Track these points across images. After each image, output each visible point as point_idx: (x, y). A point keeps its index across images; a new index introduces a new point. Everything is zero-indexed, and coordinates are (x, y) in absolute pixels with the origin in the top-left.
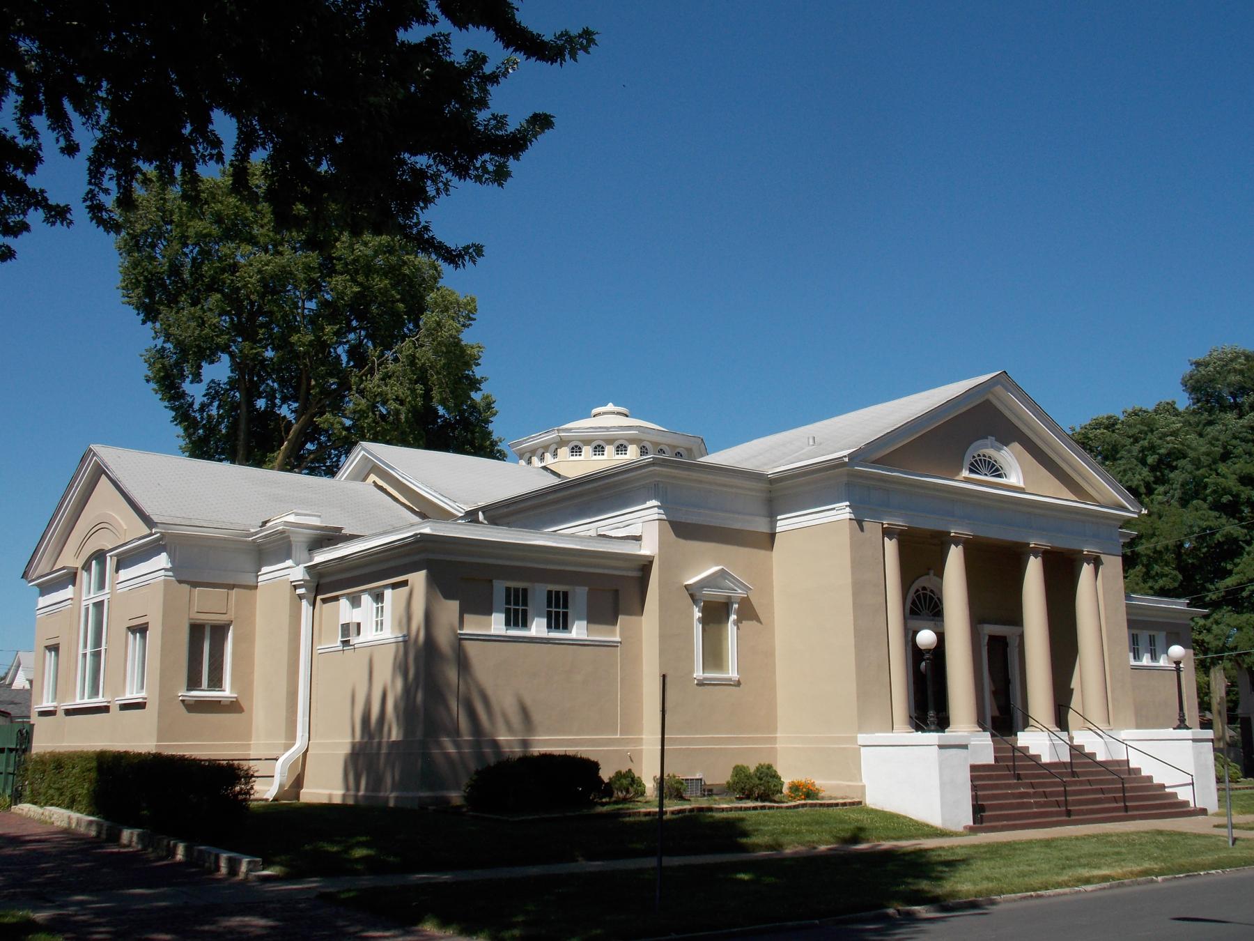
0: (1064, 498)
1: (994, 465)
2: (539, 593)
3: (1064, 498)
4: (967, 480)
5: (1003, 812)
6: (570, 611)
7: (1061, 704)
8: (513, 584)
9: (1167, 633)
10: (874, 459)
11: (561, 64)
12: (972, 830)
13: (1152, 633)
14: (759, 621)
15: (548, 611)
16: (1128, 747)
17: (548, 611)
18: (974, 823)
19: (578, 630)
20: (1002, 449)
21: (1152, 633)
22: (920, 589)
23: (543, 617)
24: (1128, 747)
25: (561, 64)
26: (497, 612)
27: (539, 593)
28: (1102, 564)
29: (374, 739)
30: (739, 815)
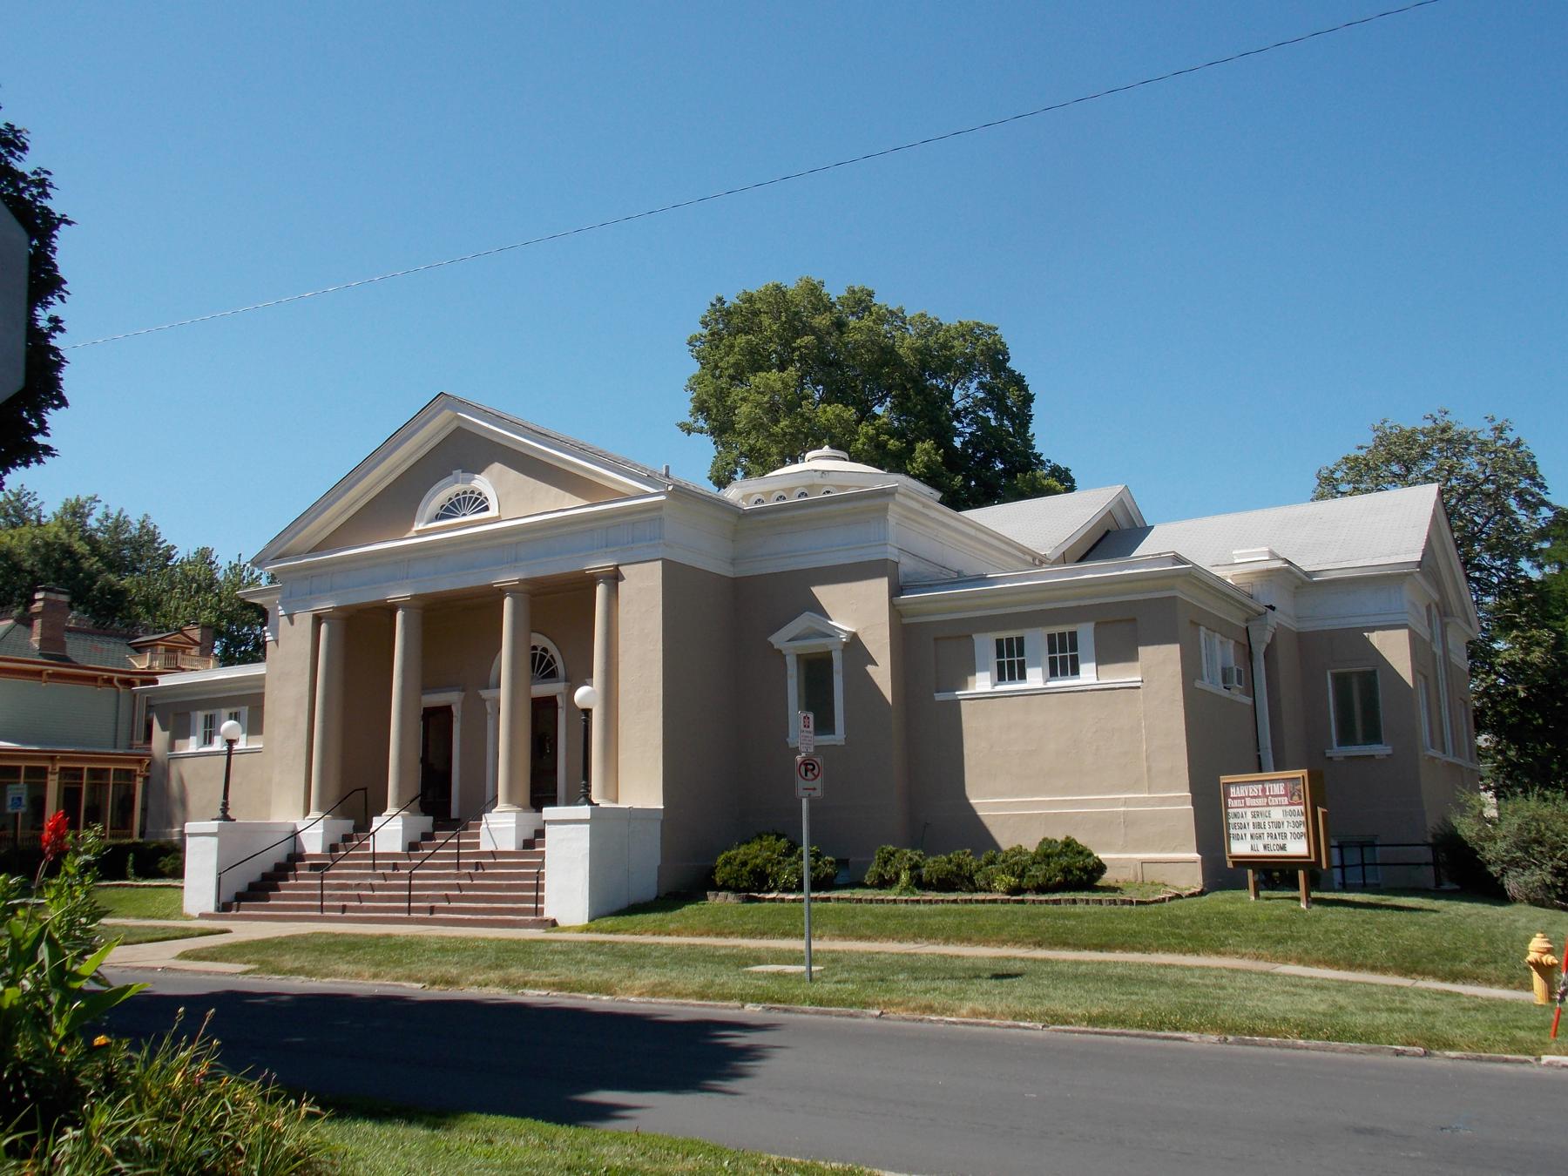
0: (568, 505)
1: (453, 504)
2: (1036, 640)
3: (568, 505)
4: (421, 533)
5: (285, 903)
6: (1079, 653)
7: (368, 790)
8: (1056, 630)
9: (1097, 624)
10: (311, 548)
11: (67, 362)
12: (586, 929)
13: (209, 712)
14: (877, 665)
15: (1022, 655)
16: (293, 838)
17: (1076, 650)
18: (215, 911)
19: (1088, 674)
20: (474, 479)
21: (209, 712)
22: (539, 649)
23: (1090, 661)
24: (293, 838)
25: (67, 362)
26: (981, 671)
27: (1036, 640)
28: (623, 579)
29: (173, 828)
30: (1045, 909)
